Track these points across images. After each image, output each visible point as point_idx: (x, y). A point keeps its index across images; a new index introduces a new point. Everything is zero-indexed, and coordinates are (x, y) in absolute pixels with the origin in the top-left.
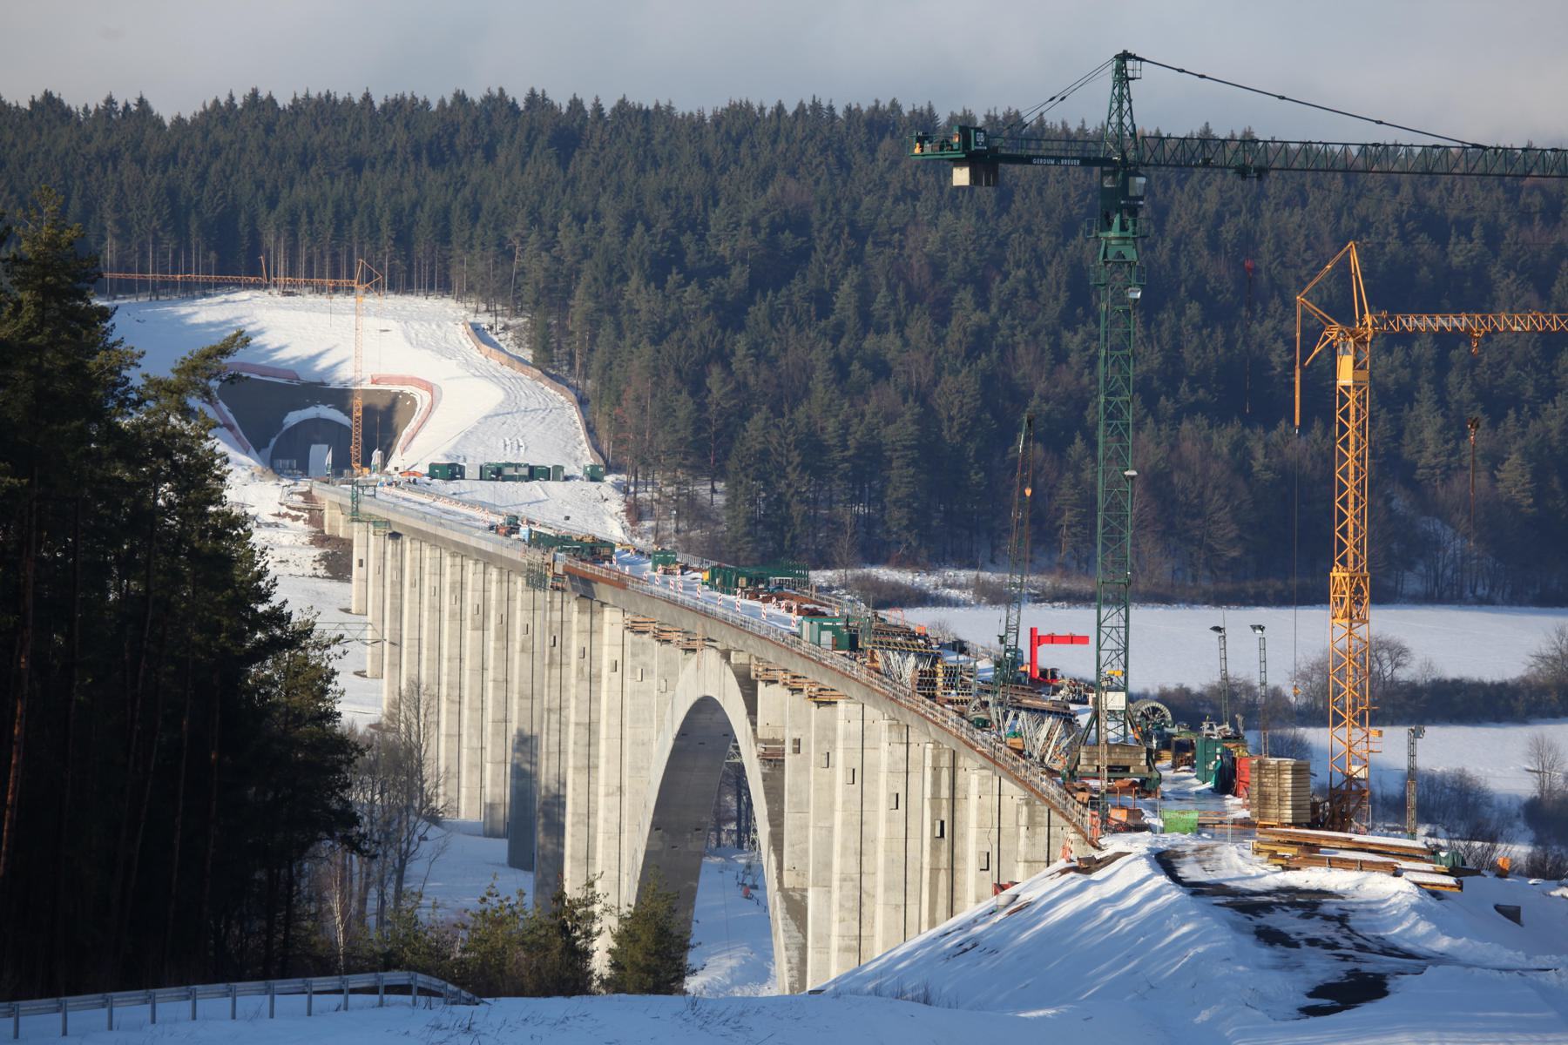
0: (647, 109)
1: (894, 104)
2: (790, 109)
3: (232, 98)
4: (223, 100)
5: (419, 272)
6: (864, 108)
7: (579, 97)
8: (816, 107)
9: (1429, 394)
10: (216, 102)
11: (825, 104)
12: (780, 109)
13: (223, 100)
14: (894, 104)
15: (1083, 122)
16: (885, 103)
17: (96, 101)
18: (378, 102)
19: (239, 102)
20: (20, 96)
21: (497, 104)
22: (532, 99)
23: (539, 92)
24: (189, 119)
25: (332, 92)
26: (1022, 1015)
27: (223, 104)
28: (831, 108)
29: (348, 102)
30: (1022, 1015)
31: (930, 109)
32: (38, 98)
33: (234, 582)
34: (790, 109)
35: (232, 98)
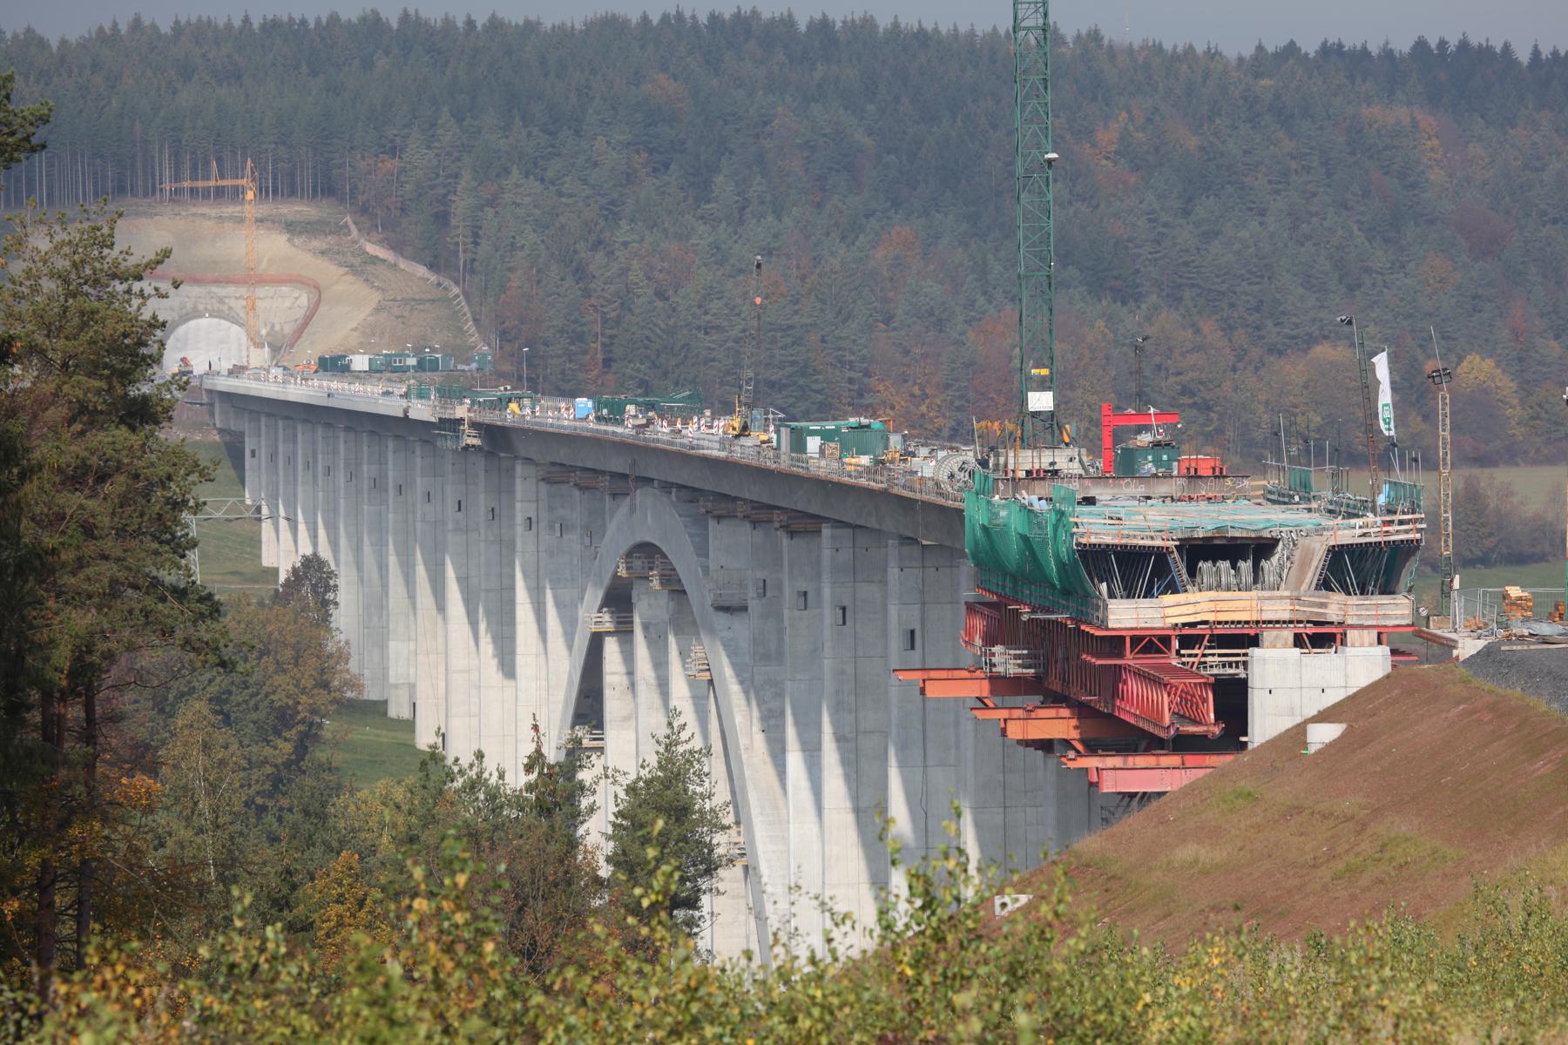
0: (517, 25)
1: (754, 12)
2: (655, 19)
3: (115, 24)
4: (107, 27)
5: (302, 175)
6: (727, 17)
7: (473, 18)
8: (679, 16)
9: (1125, 310)
10: (101, 29)
11: (687, 14)
12: (645, 19)
13: (107, 27)
14: (754, 12)
15: (972, 25)
16: (297, 17)
17: (1248, 51)
18: (256, 23)
19: (123, 28)
20: (14, 26)
21: (373, 25)
22: (405, 18)
23: (412, 12)
24: (74, 42)
25: (212, 18)
26: (481, 610)
27: (108, 31)
28: (694, 17)
29: (229, 26)
30: (481, 610)
31: (790, 15)
32: (1084, 32)
33: (690, 1032)
34: (655, 19)
35: (115, 24)
